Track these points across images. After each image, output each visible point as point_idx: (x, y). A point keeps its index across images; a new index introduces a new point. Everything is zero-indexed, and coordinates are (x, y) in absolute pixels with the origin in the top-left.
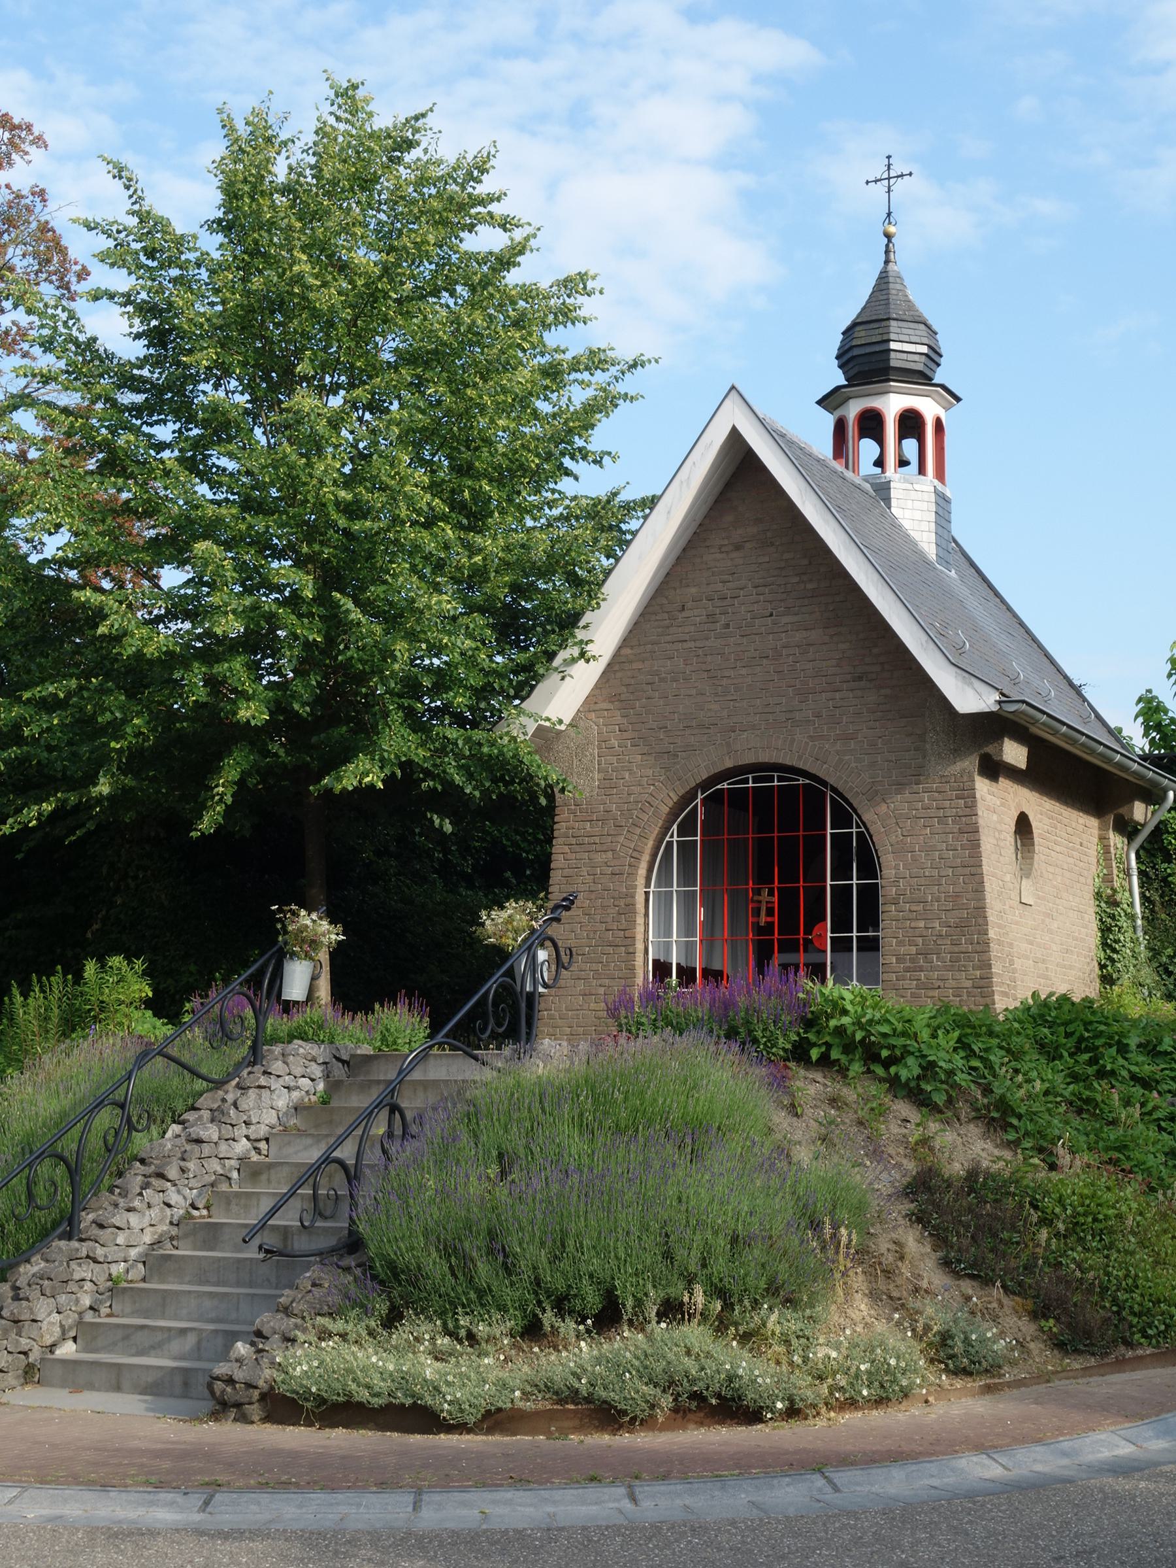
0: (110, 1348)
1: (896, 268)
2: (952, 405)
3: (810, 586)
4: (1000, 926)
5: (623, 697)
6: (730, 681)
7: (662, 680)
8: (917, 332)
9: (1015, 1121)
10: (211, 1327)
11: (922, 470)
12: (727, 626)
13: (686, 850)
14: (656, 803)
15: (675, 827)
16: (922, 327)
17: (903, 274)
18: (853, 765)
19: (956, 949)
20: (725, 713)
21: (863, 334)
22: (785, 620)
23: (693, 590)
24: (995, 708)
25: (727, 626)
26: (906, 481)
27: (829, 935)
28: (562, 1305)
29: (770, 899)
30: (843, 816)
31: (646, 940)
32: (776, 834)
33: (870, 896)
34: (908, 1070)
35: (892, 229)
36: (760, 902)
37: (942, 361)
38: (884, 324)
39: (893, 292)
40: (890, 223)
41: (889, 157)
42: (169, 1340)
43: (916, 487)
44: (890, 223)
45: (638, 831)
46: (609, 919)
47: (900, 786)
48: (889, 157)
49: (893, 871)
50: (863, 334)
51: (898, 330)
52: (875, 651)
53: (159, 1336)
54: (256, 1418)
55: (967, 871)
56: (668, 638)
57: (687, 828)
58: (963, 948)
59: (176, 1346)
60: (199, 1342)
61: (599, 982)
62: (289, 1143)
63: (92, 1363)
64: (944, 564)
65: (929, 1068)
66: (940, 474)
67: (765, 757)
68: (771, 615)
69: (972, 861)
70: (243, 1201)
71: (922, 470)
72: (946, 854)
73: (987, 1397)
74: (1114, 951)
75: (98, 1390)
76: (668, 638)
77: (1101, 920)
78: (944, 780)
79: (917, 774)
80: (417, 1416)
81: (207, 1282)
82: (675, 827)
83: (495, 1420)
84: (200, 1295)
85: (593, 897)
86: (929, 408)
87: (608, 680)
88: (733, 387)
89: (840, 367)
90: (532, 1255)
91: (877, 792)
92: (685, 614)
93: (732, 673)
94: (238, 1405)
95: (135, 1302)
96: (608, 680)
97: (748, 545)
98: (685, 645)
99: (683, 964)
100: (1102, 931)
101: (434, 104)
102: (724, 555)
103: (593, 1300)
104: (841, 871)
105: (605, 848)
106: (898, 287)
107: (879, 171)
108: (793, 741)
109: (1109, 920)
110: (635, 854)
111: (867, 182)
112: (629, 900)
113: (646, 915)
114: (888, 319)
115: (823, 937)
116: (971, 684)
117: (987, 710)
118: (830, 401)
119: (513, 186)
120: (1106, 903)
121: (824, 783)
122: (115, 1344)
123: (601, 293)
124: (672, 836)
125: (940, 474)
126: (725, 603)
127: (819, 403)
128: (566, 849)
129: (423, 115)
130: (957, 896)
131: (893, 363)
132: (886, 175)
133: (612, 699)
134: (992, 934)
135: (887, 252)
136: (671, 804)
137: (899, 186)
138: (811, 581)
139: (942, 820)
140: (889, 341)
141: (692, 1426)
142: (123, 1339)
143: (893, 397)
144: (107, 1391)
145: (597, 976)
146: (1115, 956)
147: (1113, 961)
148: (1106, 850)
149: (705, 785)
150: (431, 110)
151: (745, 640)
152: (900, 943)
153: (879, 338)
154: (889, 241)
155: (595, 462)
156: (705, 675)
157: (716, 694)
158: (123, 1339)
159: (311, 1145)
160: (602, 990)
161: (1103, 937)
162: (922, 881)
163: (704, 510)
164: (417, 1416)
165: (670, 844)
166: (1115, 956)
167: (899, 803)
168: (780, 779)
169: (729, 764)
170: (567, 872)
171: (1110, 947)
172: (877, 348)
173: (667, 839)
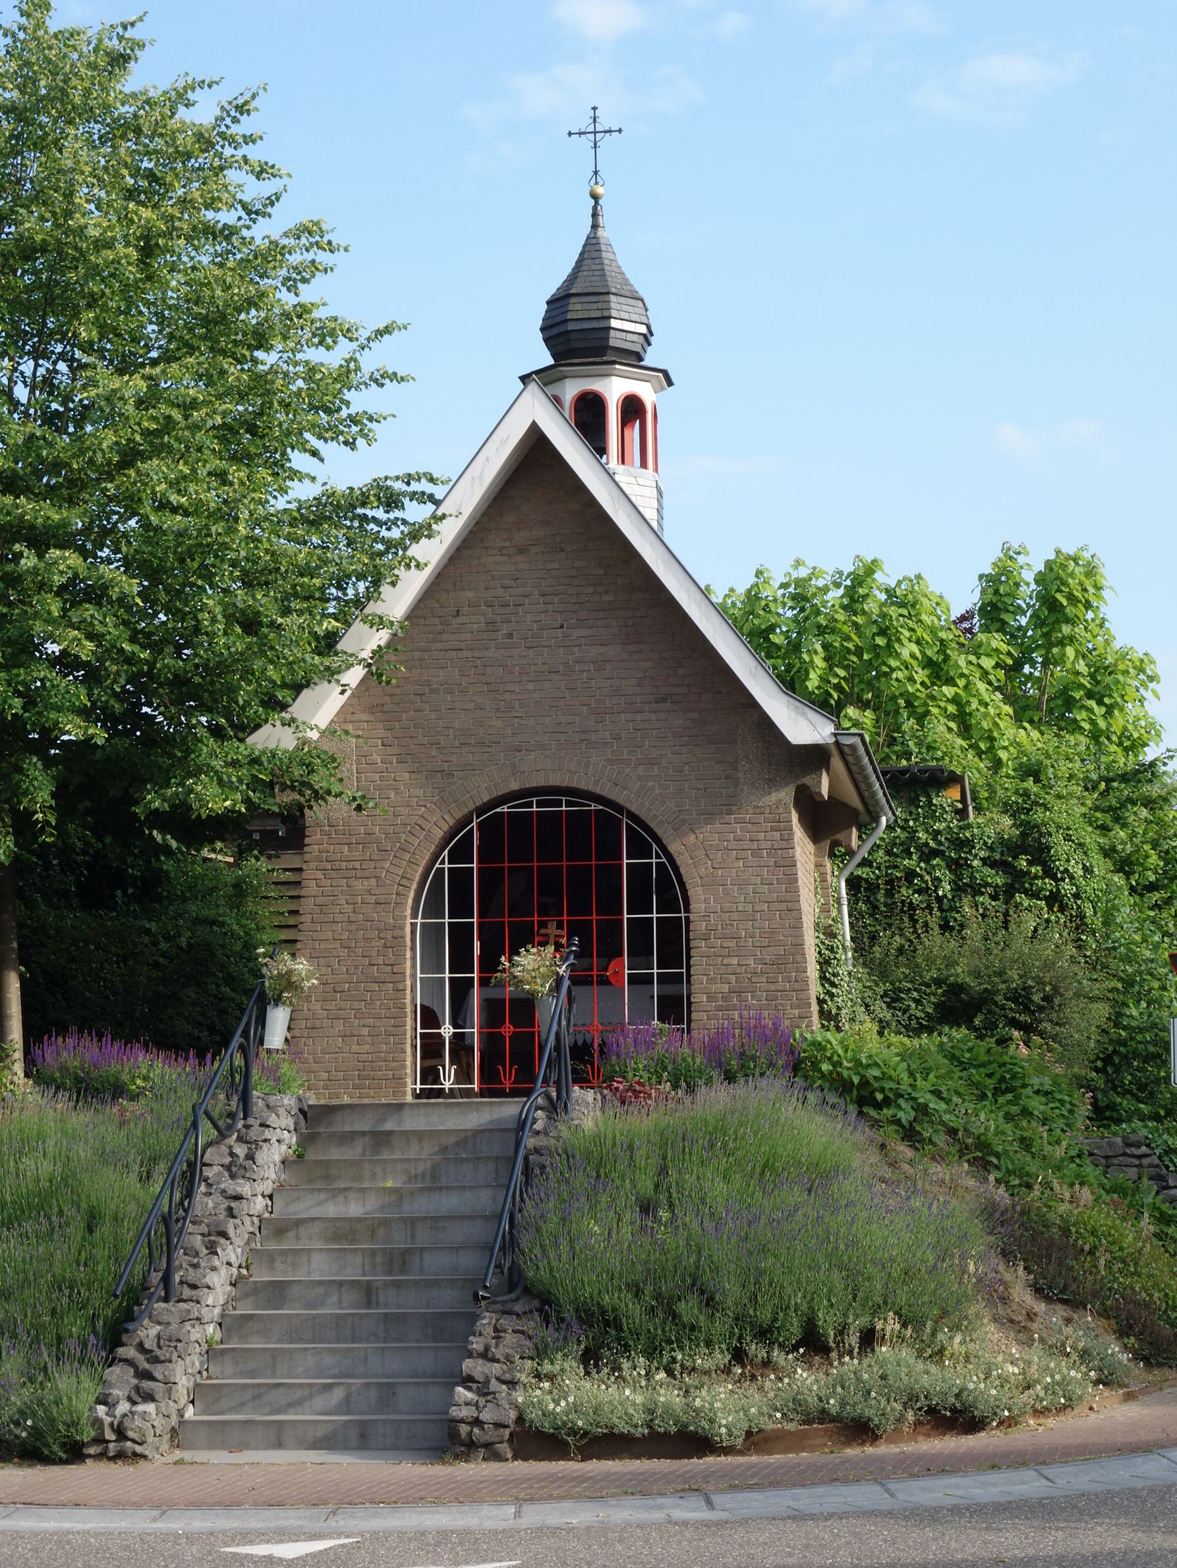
0: (240, 1407)
1: (605, 234)
2: (663, 389)
3: (605, 598)
5: (386, 708)
6: (513, 696)
7: (432, 691)
8: (637, 310)
9: (995, 1161)
10: (363, 1381)
11: (644, 464)
12: (510, 636)
14: (427, 826)
15: (446, 852)
18: (658, 792)
19: (773, 987)
20: (509, 731)
21: (579, 307)
22: (577, 633)
23: (470, 594)
25: (510, 636)
26: (630, 474)
27: (627, 971)
28: (764, 1334)
29: (558, 932)
31: (414, 976)
32: (655, 915)
34: (906, 1114)
35: (600, 190)
36: (547, 935)
38: (601, 298)
39: (606, 262)
40: (596, 183)
42: (311, 1396)
43: (640, 481)
45: (407, 856)
46: (374, 953)
47: (710, 816)
48: (594, 109)
49: (703, 904)
50: (579, 307)
51: (618, 307)
52: (680, 671)
53: (299, 1394)
54: (509, 1455)
55: (784, 906)
56: (440, 646)
58: (780, 986)
59: (319, 1402)
60: (348, 1396)
61: (362, 1022)
62: (298, 1199)
63: (246, 1422)
65: (922, 1110)
66: (656, 470)
67: (556, 780)
68: (562, 627)
69: (789, 896)
70: (290, 1259)
71: (644, 464)
72: (760, 888)
73: (1129, 1403)
74: (833, 985)
75: (255, 1448)
76: (440, 646)
77: (820, 953)
78: (758, 811)
79: (730, 804)
80: (691, 1442)
81: (300, 1340)
82: (446, 852)
83: (756, 1440)
84: (318, 1352)
85: (353, 927)
86: (646, 392)
87: (367, 689)
90: (731, 1291)
91: (684, 821)
92: (460, 620)
93: (517, 688)
94: (487, 1445)
95: (238, 1363)
96: (367, 689)
97: (534, 549)
98: (460, 654)
99: (427, 1004)
100: (820, 963)
101: (146, 13)
102: (506, 558)
103: (794, 1329)
104: (639, 903)
105: (367, 874)
106: (611, 256)
108: (588, 764)
109: (827, 952)
110: (404, 882)
111: (570, 134)
112: (397, 933)
113: (413, 949)
114: (608, 293)
115: (619, 974)
116: (805, 714)
117: (822, 742)
119: (274, 134)
120: (824, 934)
121: (619, 808)
122: (243, 1404)
123: (346, 250)
124: (443, 862)
125: (656, 470)
126: (508, 610)
128: (320, 875)
129: (133, 24)
130: (773, 932)
131: (612, 343)
133: (372, 709)
135: (595, 215)
137: (605, 142)
138: (606, 592)
139: (756, 853)
140: (610, 317)
141: (921, 1438)
142: (253, 1399)
143: (615, 380)
144: (266, 1448)
145: (359, 1015)
146: (834, 990)
147: (832, 995)
148: (823, 876)
149: (480, 811)
150: (141, 19)
151: (531, 652)
152: (711, 981)
153: (598, 314)
154: (597, 203)
155: (346, 443)
156: (485, 688)
157: (498, 710)
158: (253, 1399)
159: (326, 1201)
160: (365, 1031)
161: (821, 970)
162: (735, 916)
163: (486, 506)
164: (691, 1442)
165: (440, 871)
166: (834, 990)
167: (710, 833)
168: (568, 804)
169: (514, 786)
170: (320, 900)
171: (828, 980)
172: (595, 325)
173: (437, 865)
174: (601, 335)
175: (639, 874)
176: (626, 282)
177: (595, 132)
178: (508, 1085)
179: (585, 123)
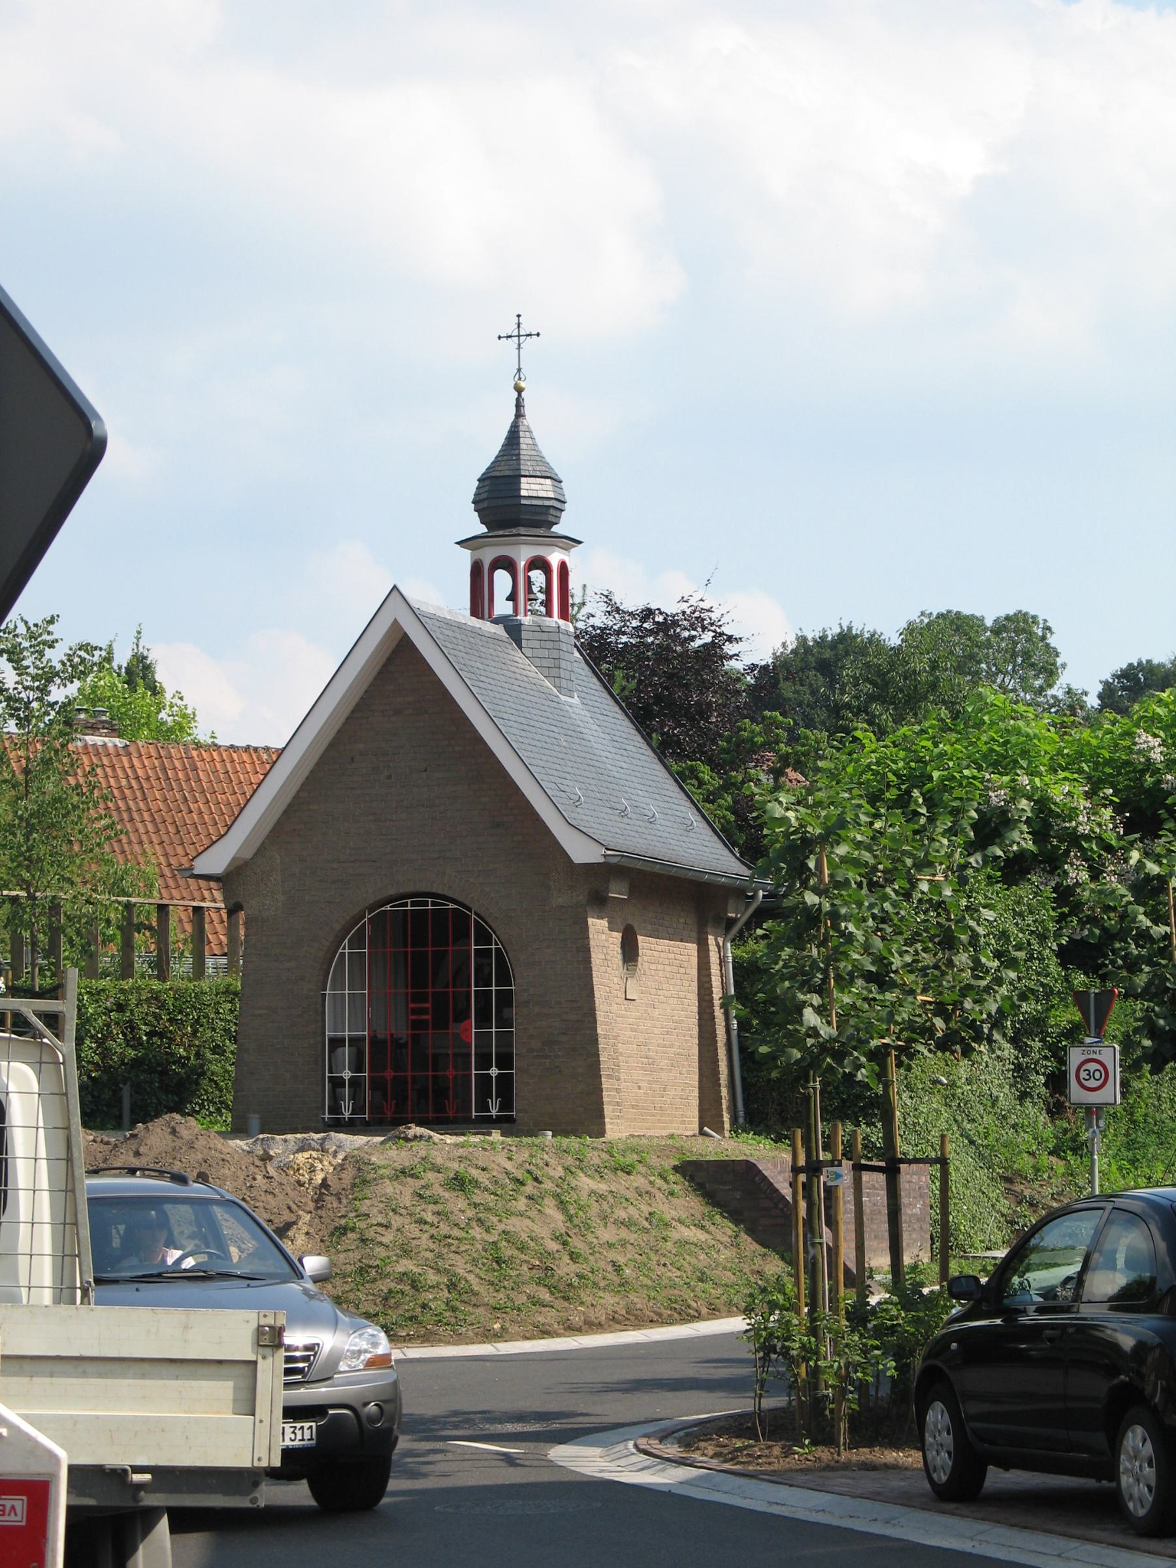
4: (606, 1024)
12: (389, 777)
13: (357, 959)
16: (548, 481)
23: (361, 746)
24: (602, 860)
30: (484, 936)
32: (494, 988)
33: (505, 999)
35: (522, 384)
40: (520, 379)
48: (519, 316)
57: (357, 942)
88: (395, 587)
104: (483, 979)
134: (599, 1031)
135: (519, 405)
137: (527, 343)
149: (371, 909)
168: (434, 904)
169: (392, 891)
176: (541, 460)
177: (519, 336)
178: (389, 1115)
179: (511, 329)
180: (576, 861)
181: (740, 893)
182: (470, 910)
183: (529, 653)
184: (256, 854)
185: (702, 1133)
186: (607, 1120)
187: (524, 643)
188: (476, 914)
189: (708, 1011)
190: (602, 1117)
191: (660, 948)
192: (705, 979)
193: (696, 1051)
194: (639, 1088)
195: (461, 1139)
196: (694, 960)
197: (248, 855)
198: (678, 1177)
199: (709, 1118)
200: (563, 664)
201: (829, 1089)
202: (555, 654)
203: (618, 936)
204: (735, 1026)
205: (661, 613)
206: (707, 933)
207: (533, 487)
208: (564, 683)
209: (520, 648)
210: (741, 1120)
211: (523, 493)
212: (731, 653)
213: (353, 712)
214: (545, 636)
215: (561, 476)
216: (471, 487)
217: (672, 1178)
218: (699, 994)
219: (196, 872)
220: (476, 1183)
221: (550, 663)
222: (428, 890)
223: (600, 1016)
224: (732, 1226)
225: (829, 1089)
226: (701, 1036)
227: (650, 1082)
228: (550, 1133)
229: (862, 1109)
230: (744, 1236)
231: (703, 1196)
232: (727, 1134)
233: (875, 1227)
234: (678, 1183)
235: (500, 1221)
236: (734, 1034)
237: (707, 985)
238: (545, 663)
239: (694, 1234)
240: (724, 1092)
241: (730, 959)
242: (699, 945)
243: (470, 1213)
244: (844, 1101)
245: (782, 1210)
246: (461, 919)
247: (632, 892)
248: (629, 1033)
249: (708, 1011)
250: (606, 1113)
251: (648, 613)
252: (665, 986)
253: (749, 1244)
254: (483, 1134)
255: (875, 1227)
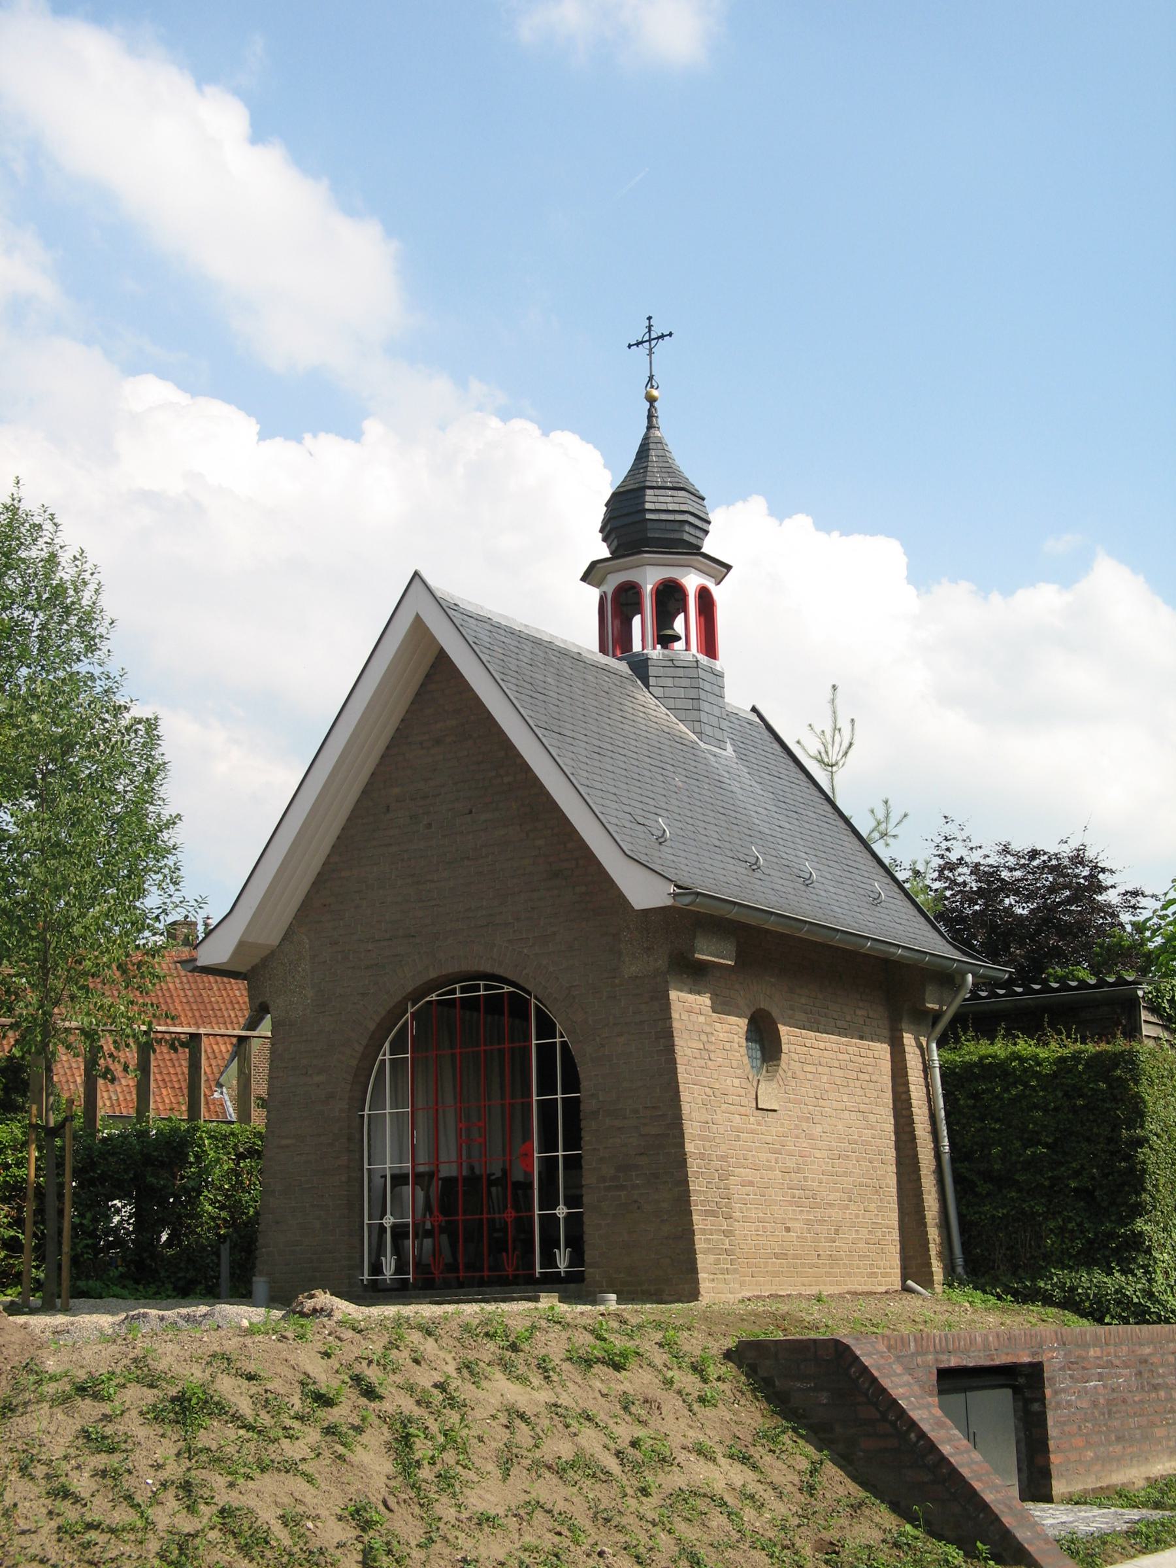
12: (429, 826)
15: (387, 1045)
17: (667, 440)
23: (396, 791)
24: (669, 902)
30: (546, 1027)
33: (572, 1107)
35: (655, 393)
37: (711, 528)
40: (652, 387)
41: (649, 318)
44: (652, 387)
48: (649, 318)
64: (715, 742)
68: (471, 812)
82: (387, 1045)
88: (416, 574)
89: (604, 540)
104: (547, 1086)
107: (640, 333)
118: (592, 574)
127: (584, 579)
132: (646, 338)
134: (689, 1147)
135: (650, 417)
136: (377, 1019)
149: (415, 996)
154: (652, 405)
168: (487, 988)
169: (433, 975)
173: (380, 1057)
174: (699, 534)
175: (546, 1053)
176: (671, 471)
180: (637, 907)
181: (947, 978)
182: (529, 994)
183: (658, 692)
184: (283, 939)
185: (906, 1289)
186: (702, 1276)
187: (652, 681)
188: (536, 998)
189: (907, 1129)
190: (694, 1270)
191: (822, 1046)
192: (901, 1089)
193: (892, 1181)
194: (788, 1230)
195: (638, 1307)
196: (886, 1066)
197: (271, 937)
198: (729, 1369)
199: (914, 1268)
200: (705, 706)
201: (1070, 1226)
202: (693, 693)
203: (739, 1024)
204: (947, 1149)
205: (1045, 853)
206: (901, 1031)
207: (662, 499)
208: (708, 730)
209: (647, 686)
210: (960, 1270)
211: (648, 506)
212: (1109, 884)
213: (388, 748)
214: (680, 672)
215: (702, 493)
216: (598, 513)
217: (713, 1371)
218: (895, 1109)
219: (199, 963)
220: (216, 1408)
221: (689, 704)
222: (475, 968)
223: (691, 1128)
224: (810, 1449)
225: (1070, 1226)
226: (899, 1163)
227: (807, 1222)
228: (613, 1297)
229: (1116, 1251)
230: (831, 1470)
231: (769, 1400)
232: (939, 1288)
233: (1116, 1423)
234: (727, 1381)
235: (231, 1485)
236: (946, 1158)
237: (904, 1097)
238: (679, 704)
239: (722, 1476)
240: (933, 1234)
241: (937, 1064)
242: (892, 1045)
243: (175, 1470)
244: (1091, 1242)
245: (893, 1424)
246: (518, 1006)
247: (740, 957)
248: (764, 1156)
249: (907, 1129)
250: (699, 1266)
251: (1034, 854)
252: (832, 1095)
253: (837, 1484)
254: (529, 1299)
255: (1116, 1423)
